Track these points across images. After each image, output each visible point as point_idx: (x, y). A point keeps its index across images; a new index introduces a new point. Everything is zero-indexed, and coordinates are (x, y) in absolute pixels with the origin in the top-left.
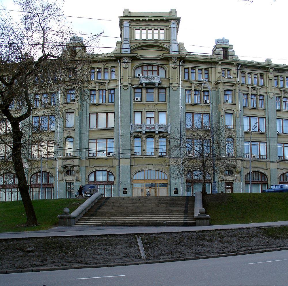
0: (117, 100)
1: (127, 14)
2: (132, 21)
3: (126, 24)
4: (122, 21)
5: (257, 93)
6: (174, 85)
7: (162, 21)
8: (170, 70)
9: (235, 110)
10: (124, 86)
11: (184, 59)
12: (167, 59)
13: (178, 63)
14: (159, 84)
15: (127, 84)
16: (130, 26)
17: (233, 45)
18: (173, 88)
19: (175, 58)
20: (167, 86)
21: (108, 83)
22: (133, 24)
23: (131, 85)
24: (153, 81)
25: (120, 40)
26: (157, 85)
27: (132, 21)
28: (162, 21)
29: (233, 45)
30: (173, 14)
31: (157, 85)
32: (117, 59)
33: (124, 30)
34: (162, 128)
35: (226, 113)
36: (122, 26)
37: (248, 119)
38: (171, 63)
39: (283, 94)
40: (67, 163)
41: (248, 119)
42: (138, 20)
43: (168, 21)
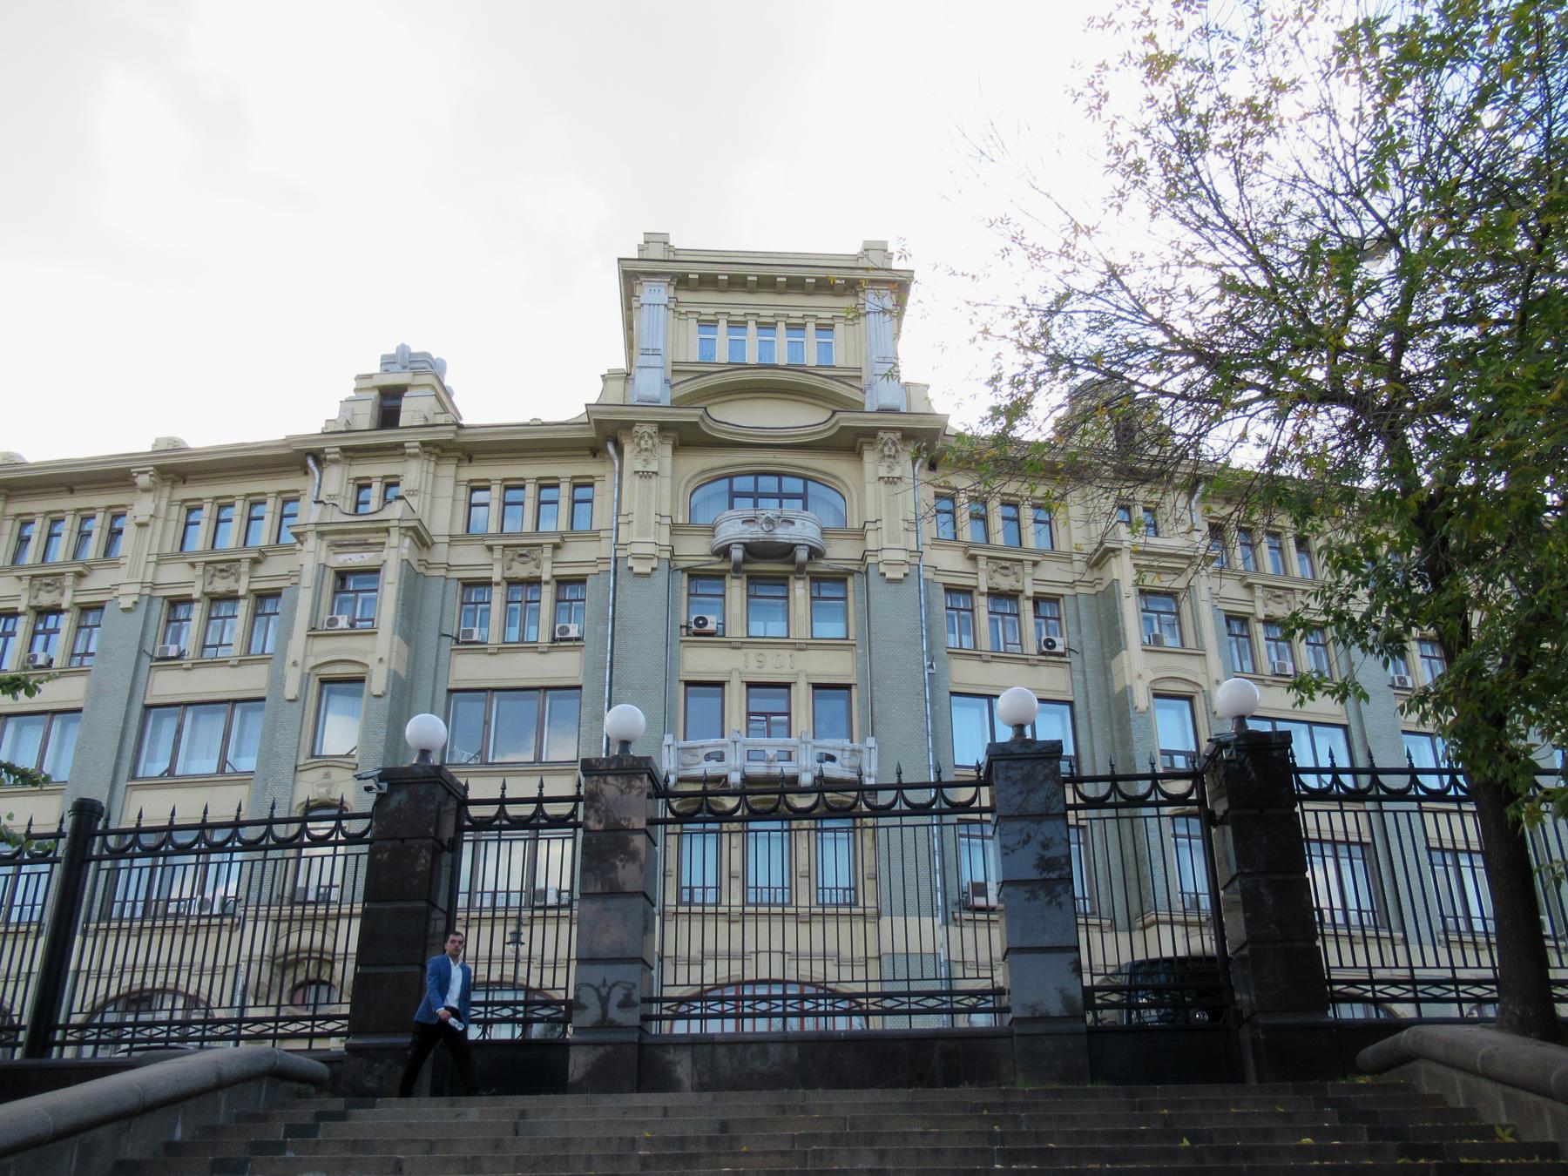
0: (600, 629)
1: (656, 252)
2: (681, 282)
3: (655, 294)
4: (632, 277)
5: (1018, 586)
6: (886, 555)
7: (823, 286)
8: (870, 491)
9: (1201, 680)
10: (637, 557)
11: (927, 443)
12: (850, 444)
13: (905, 459)
14: (815, 553)
15: (652, 549)
16: (672, 305)
17: (927, 386)
18: (882, 569)
19: (891, 435)
20: (855, 568)
21: (556, 547)
22: (685, 296)
23: (672, 553)
24: (783, 534)
25: (620, 363)
26: (802, 555)
27: (681, 282)
28: (823, 286)
29: (927, 386)
30: (876, 260)
31: (802, 555)
32: (603, 436)
33: (642, 320)
34: (832, 758)
35: (1156, 696)
36: (635, 304)
37: (982, 709)
38: (869, 457)
39: (1259, 604)
40: (305, 938)
41: (982, 709)
42: (708, 282)
43: (863, 286)
